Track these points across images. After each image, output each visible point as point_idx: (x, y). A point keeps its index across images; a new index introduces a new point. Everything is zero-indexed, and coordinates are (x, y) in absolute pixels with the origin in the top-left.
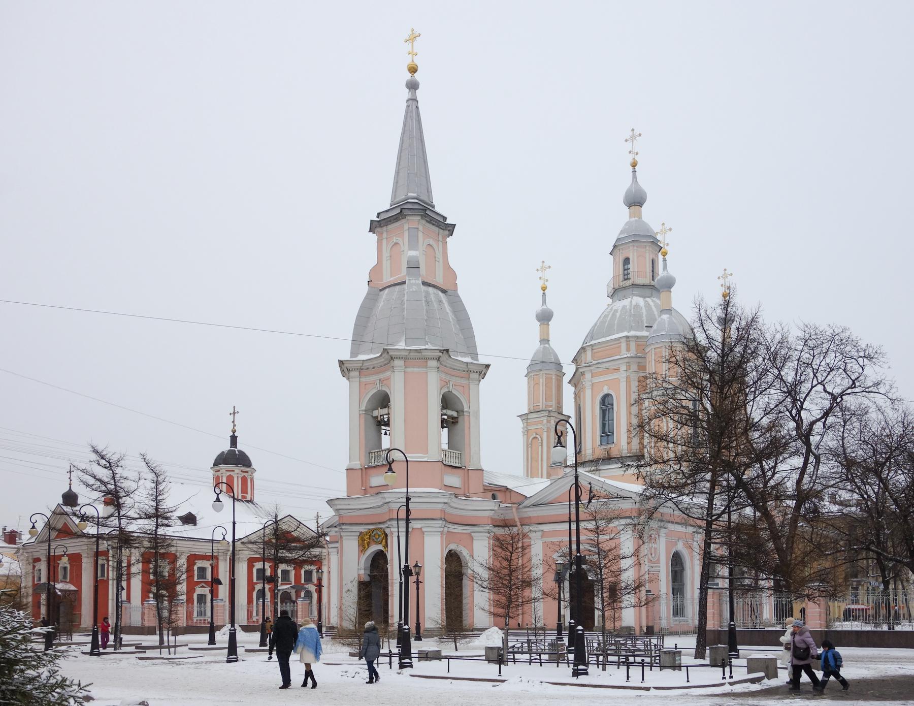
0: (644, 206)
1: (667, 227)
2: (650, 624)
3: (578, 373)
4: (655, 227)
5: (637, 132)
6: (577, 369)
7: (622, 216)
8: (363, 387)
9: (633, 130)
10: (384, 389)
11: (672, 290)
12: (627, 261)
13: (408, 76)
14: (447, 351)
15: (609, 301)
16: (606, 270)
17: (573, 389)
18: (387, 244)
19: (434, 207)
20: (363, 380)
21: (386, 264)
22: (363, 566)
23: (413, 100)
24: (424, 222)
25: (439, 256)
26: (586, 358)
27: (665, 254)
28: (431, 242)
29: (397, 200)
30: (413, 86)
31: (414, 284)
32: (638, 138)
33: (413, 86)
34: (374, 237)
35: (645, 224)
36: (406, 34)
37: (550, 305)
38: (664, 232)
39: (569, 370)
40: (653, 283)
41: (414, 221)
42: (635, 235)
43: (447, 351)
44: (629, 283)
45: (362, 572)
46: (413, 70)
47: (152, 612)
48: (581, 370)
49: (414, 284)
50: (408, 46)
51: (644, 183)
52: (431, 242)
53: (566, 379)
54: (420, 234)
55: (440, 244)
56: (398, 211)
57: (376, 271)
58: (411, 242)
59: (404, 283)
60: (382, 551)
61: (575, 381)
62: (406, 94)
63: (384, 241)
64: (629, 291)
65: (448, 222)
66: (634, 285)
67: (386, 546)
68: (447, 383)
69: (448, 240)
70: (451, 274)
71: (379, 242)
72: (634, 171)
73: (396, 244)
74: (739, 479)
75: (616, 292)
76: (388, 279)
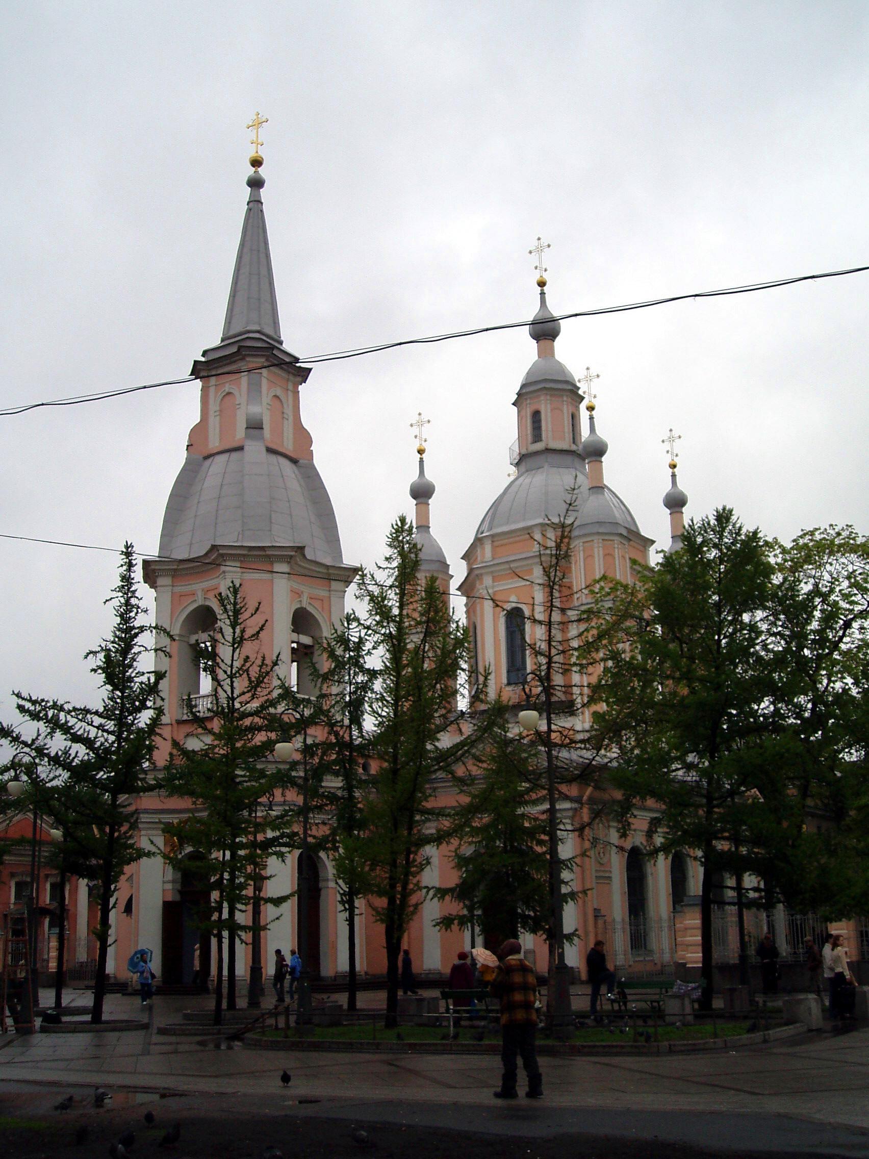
0: (558, 339)
1: (593, 372)
2: (600, 938)
3: (471, 578)
4: (576, 372)
5: (425, 417)
6: (471, 571)
8: (177, 599)
9: (539, 239)
10: (208, 603)
11: (603, 459)
12: (536, 415)
14: (301, 549)
16: (506, 428)
17: (464, 599)
18: (216, 393)
19: (281, 343)
20: (177, 589)
21: (214, 422)
23: (255, 204)
25: (289, 411)
26: (483, 555)
27: (591, 408)
28: (279, 392)
29: (231, 333)
30: (256, 184)
31: (255, 451)
32: (546, 250)
33: (256, 184)
35: (561, 368)
36: (250, 118)
37: (429, 476)
38: (589, 379)
39: (458, 572)
40: (574, 448)
42: (545, 380)
43: (301, 549)
44: (539, 446)
45: (169, 886)
46: (256, 163)
48: (477, 572)
49: (255, 451)
50: (251, 134)
52: (279, 392)
53: (454, 584)
54: (264, 382)
55: (290, 393)
56: (234, 349)
57: (197, 435)
58: (251, 396)
59: (241, 449)
61: (466, 588)
63: (212, 390)
64: (542, 458)
66: (548, 450)
68: (299, 594)
70: (304, 438)
71: (204, 390)
72: (542, 294)
73: (229, 393)
74: (349, 788)
75: (523, 460)
76: (214, 443)
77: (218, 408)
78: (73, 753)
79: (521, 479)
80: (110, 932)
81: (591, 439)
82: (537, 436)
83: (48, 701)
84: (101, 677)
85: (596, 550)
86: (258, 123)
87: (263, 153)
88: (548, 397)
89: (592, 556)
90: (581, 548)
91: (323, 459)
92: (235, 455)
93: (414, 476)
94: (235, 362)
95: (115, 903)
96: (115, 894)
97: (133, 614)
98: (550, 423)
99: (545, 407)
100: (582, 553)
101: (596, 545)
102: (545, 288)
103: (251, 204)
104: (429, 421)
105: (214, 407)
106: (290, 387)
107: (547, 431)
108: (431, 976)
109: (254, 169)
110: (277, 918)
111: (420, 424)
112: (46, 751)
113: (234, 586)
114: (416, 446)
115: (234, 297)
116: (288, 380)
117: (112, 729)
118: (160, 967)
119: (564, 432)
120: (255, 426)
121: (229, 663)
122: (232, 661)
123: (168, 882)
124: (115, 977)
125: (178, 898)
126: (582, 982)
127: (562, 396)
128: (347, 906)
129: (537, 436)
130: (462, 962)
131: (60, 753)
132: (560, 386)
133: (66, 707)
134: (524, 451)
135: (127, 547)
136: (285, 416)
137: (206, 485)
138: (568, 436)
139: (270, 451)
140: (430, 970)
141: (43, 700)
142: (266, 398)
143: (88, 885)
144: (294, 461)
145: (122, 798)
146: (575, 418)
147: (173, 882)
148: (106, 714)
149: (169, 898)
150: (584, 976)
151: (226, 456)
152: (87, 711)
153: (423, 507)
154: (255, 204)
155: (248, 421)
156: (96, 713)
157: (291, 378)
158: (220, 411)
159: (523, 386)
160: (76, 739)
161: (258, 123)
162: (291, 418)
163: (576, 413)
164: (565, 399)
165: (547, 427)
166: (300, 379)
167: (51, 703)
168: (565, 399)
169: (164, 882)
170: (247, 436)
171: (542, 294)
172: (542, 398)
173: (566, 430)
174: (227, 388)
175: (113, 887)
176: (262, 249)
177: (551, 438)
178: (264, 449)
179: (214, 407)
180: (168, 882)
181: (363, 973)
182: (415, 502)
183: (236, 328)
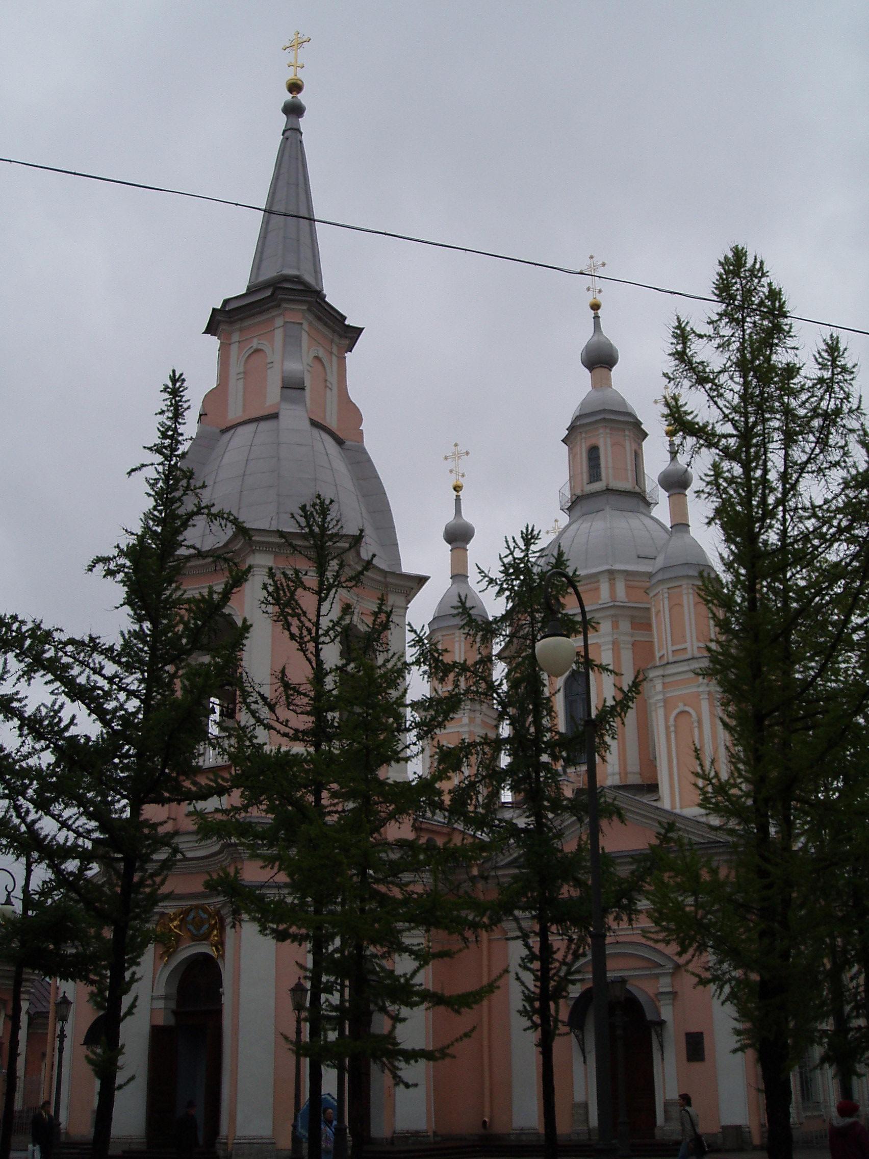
5: (462, 449)
7: (579, 385)
9: (592, 257)
12: (593, 453)
13: (289, 96)
15: (564, 519)
21: (236, 386)
22: (161, 991)
24: (310, 317)
25: (333, 379)
28: (321, 353)
29: (262, 279)
30: (294, 110)
31: (294, 418)
33: (294, 110)
34: (214, 342)
37: (468, 516)
41: (296, 313)
42: (600, 412)
45: (160, 1004)
46: (295, 87)
47: (686, 383)
49: (294, 418)
51: (612, 334)
52: (321, 353)
54: (305, 336)
55: (334, 359)
56: (268, 293)
58: (285, 349)
59: (275, 416)
60: (206, 957)
62: (282, 120)
63: (234, 348)
65: (347, 323)
66: (609, 491)
67: (220, 945)
69: (348, 355)
70: (352, 414)
71: (224, 350)
72: (596, 317)
73: (257, 351)
76: (235, 413)
77: (242, 369)
78: (65, 716)
79: (574, 527)
80: (121, 1060)
81: (672, 467)
82: (594, 473)
83: (23, 622)
84: (118, 591)
85: (685, 598)
86: (298, 43)
87: (302, 76)
88: (608, 431)
89: (680, 605)
90: (666, 595)
91: (375, 442)
92: (264, 425)
93: (449, 517)
94: (267, 310)
95: (133, 1005)
96: (135, 986)
97: (177, 494)
98: (610, 460)
99: (604, 441)
100: (666, 601)
101: (685, 591)
102: (599, 311)
103: (288, 134)
104: (467, 453)
105: (236, 367)
106: (335, 350)
107: (607, 468)
108: (524, 1138)
109: (291, 95)
110: (466, 1035)
111: (457, 456)
112: (15, 704)
113: (322, 503)
114: (453, 482)
115: (265, 238)
116: (332, 341)
117: (133, 687)
118: (144, 1124)
119: (626, 470)
120: (293, 387)
121: (314, 619)
122: (318, 616)
123: (158, 998)
124: (67, 1133)
125: (172, 1021)
126: (755, 1148)
127: (624, 430)
128: (536, 1018)
129: (594, 473)
130: (849, 1120)
131: (44, 711)
132: (622, 418)
133: (57, 635)
134: (579, 492)
135: (174, 380)
136: (328, 384)
137: (226, 460)
138: (631, 475)
139: (314, 424)
140: (522, 1129)
141: (14, 618)
142: (308, 358)
143: (716, 466)
144: (340, 442)
145: (182, 778)
146: (638, 456)
147: (166, 998)
148: (126, 656)
149: (160, 1021)
150: (756, 1140)
151: (251, 427)
152: (93, 645)
153: (459, 552)
154: (292, 135)
155: (284, 379)
156: (108, 652)
157: (336, 339)
158: (245, 373)
159: (578, 418)
160: (76, 692)
161: (298, 43)
162: (335, 389)
163: (639, 452)
164: (627, 433)
165: (607, 462)
166: (346, 342)
167: (30, 625)
168: (627, 433)
169: (153, 998)
170: (283, 398)
171: (596, 317)
172: (601, 431)
173: (629, 467)
174: (255, 344)
175: (127, 975)
176: (301, 185)
177: (610, 477)
178: (307, 423)
179: (236, 367)
180: (158, 998)
181: (430, 1133)
182: (449, 547)
183: (269, 273)
